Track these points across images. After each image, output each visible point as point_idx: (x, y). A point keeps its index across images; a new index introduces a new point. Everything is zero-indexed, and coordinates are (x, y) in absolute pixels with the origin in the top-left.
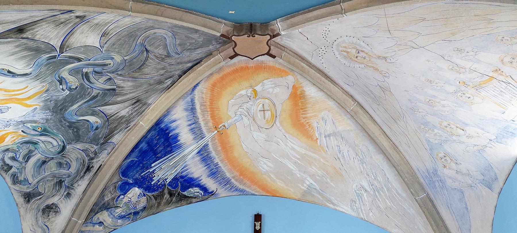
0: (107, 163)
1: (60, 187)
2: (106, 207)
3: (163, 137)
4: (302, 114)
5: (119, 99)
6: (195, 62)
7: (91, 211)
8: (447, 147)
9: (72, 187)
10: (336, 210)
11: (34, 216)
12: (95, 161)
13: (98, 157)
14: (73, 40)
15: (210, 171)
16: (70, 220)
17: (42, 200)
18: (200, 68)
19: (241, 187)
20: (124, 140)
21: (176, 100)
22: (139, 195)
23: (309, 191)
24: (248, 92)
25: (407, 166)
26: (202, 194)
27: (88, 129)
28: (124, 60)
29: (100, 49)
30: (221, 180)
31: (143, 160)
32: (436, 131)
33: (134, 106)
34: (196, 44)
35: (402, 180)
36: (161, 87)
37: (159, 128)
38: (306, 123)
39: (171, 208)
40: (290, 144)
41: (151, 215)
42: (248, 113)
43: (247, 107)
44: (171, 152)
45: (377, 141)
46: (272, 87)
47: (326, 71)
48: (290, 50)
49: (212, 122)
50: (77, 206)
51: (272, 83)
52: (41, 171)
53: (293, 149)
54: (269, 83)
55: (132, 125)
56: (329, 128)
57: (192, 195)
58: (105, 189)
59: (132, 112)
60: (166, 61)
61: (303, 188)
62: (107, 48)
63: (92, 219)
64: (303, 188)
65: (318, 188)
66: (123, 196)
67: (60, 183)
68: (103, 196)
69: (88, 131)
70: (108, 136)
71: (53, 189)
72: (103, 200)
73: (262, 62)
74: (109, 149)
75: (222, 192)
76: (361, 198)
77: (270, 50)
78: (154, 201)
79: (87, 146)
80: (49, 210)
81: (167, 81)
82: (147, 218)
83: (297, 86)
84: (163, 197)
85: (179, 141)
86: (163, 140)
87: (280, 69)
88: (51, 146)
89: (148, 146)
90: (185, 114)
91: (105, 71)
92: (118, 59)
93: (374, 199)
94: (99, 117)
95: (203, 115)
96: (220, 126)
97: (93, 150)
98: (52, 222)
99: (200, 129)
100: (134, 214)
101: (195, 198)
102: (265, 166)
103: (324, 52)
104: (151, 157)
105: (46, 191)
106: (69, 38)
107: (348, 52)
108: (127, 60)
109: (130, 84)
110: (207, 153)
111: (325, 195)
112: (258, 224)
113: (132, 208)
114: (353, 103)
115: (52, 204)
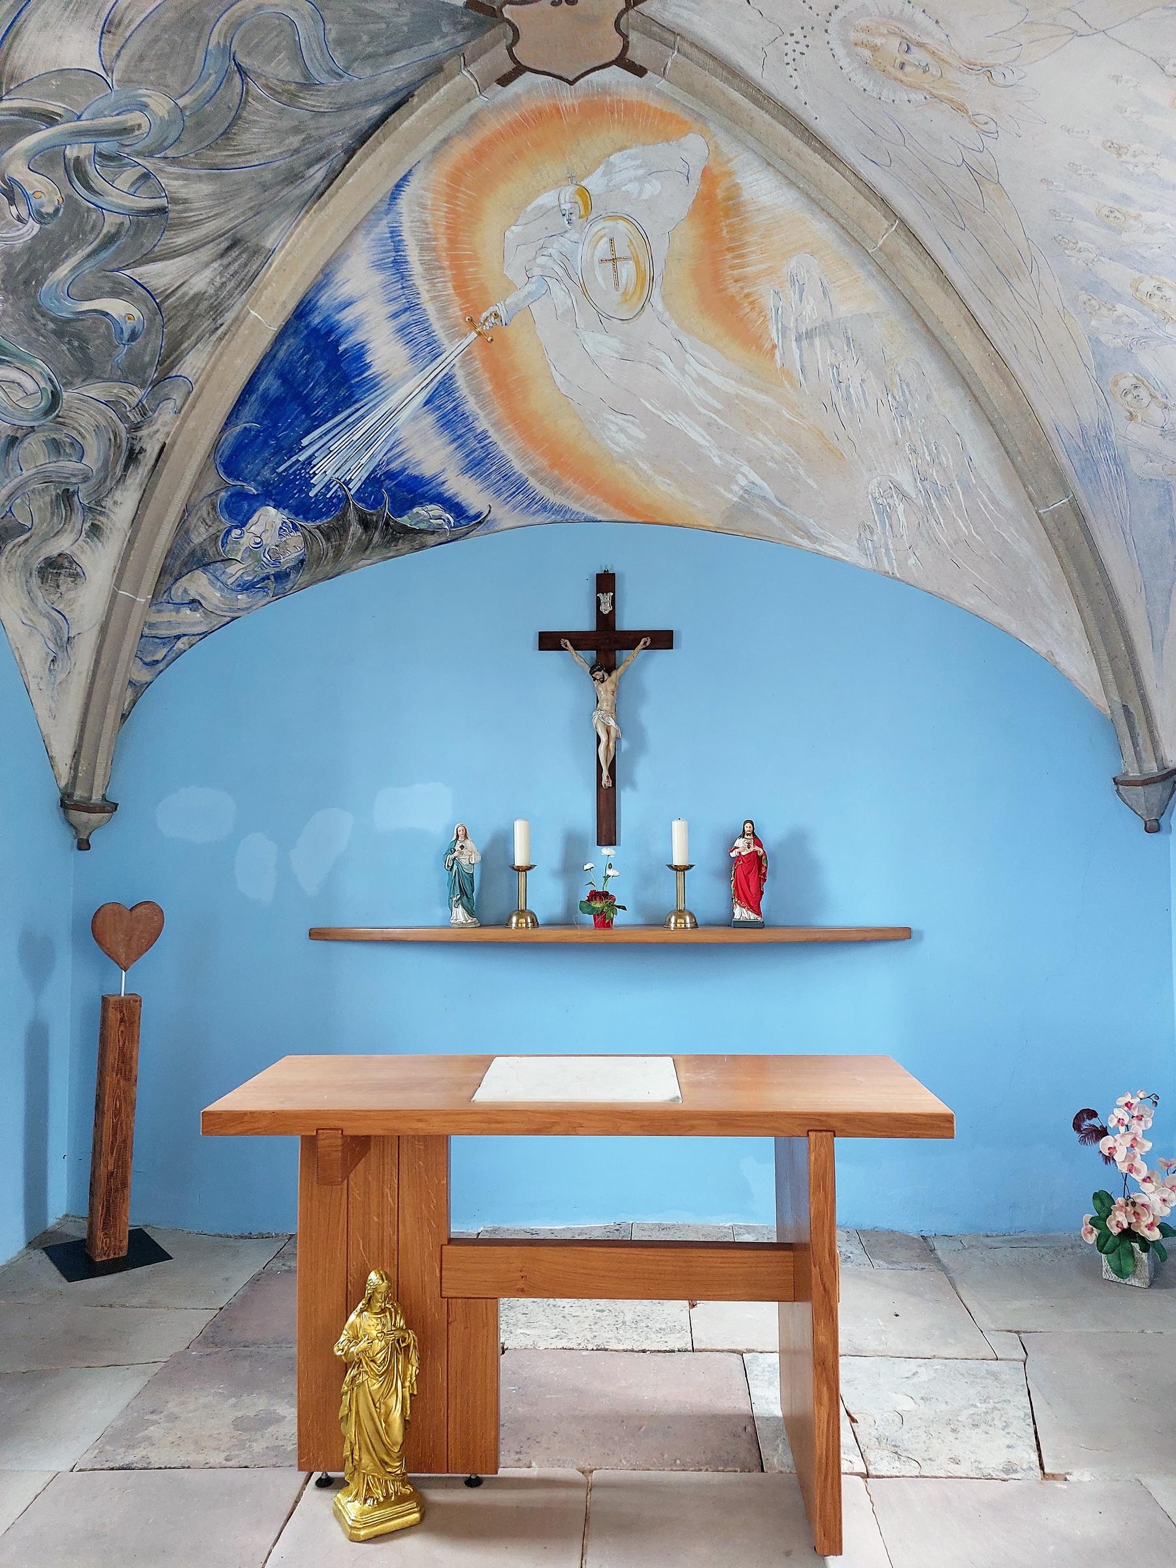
0: (180, 439)
1: (68, 508)
2: (200, 561)
3: (322, 354)
4: (730, 267)
5: (181, 240)
6: (391, 102)
7: (164, 571)
8: (1146, 360)
9: (99, 508)
10: (818, 553)
11: (22, 587)
12: (144, 432)
13: (151, 422)
14: (24, 55)
15: (467, 456)
16: (114, 596)
17: (30, 546)
18: (409, 122)
19: (555, 499)
20: (213, 368)
21: (347, 234)
22: (281, 528)
23: (745, 506)
24: (562, 198)
25: (1027, 420)
26: (450, 522)
27: (108, 337)
28: (179, 110)
29: (105, 76)
30: (498, 481)
31: (275, 426)
32: (1121, 308)
33: (225, 261)
34: (390, 37)
35: (1009, 461)
36: (297, 192)
37: (307, 327)
38: (742, 295)
39: (370, 561)
40: (693, 367)
41: (320, 580)
42: (566, 270)
43: (563, 250)
44: (348, 401)
45: (949, 346)
46: (637, 179)
47: (807, 114)
48: (692, 44)
49: (460, 305)
50: (125, 558)
51: (638, 162)
52: (10, 467)
53: (702, 381)
54: (630, 163)
55: (229, 322)
56: (811, 311)
57: (423, 526)
58: (187, 511)
59: (224, 279)
60: (303, 103)
61: (730, 496)
62: (125, 71)
63: (170, 593)
64: (730, 496)
65: (771, 496)
66: (238, 531)
67: (67, 497)
68: (187, 532)
69: (111, 343)
70: (168, 358)
71: (53, 513)
72: (189, 541)
73: (605, 90)
74: (177, 397)
75: (504, 515)
76: (890, 518)
77: (625, 48)
78: (324, 543)
79: (117, 389)
80: (55, 571)
81: (312, 171)
82: (310, 587)
83: (715, 171)
84: (346, 531)
85: (368, 367)
86: (322, 365)
87: (663, 114)
88: (22, 395)
89: (283, 384)
90: (378, 278)
91: (127, 150)
92: (160, 105)
93: (925, 519)
94: (134, 301)
95: (432, 282)
96: (485, 315)
97: (134, 401)
98: (72, 602)
99: (426, 329)
100: (275, 578)
101: (433, 533)
102: (622, 438)
103: (799, 48)
104: (296, 418)
105: (36, 521)
106: (10, 49)
107: (875, 49)
108: (185, 108)
109: (205, 188)
110: (454, 401)
111: (790, 514)
112: (606, 598)
113: (267, 562)
114: (886, 224)
115: (60, 555)
